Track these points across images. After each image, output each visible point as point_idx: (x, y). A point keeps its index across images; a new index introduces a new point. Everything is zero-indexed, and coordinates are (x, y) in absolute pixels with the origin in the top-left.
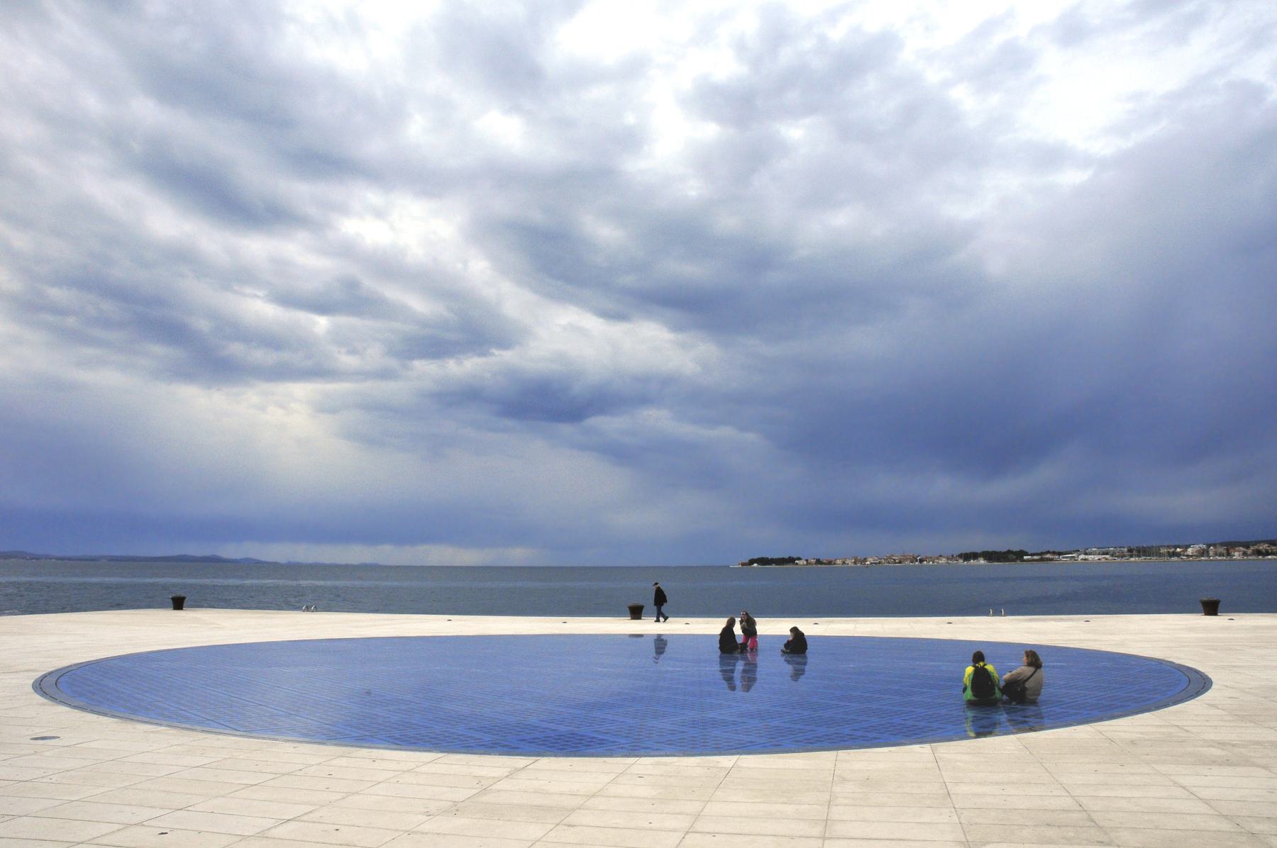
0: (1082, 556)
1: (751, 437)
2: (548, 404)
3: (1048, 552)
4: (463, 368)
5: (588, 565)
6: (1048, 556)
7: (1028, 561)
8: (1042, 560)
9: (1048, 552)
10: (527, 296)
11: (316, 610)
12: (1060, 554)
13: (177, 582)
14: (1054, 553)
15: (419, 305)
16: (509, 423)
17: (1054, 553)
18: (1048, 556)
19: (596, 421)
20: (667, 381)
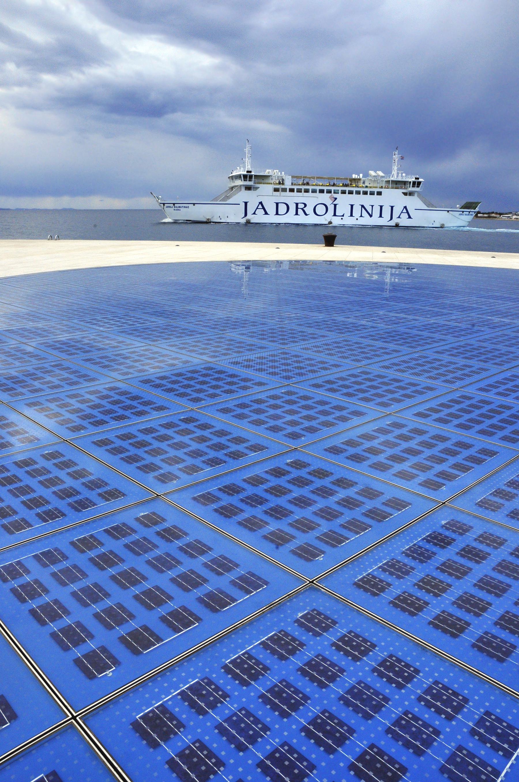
0: (515, 217)
1: (277, 128)
2: (137, 106)
3: (493, 213)
4: (77, 79)
5: (114, 208)
6: (493, 215)
7: (481, 217)
8: (489, 217)
9: (493, 213)
10: (116, 33)
11: (59, 238)
12: (500, 214)
13: (397, 232)
14: (496, 213)
15: (38, 37)
16: (115, 116)
17: (496, 213)
18: (493, 215)
19: (177, 116)
20: (215, 90)
